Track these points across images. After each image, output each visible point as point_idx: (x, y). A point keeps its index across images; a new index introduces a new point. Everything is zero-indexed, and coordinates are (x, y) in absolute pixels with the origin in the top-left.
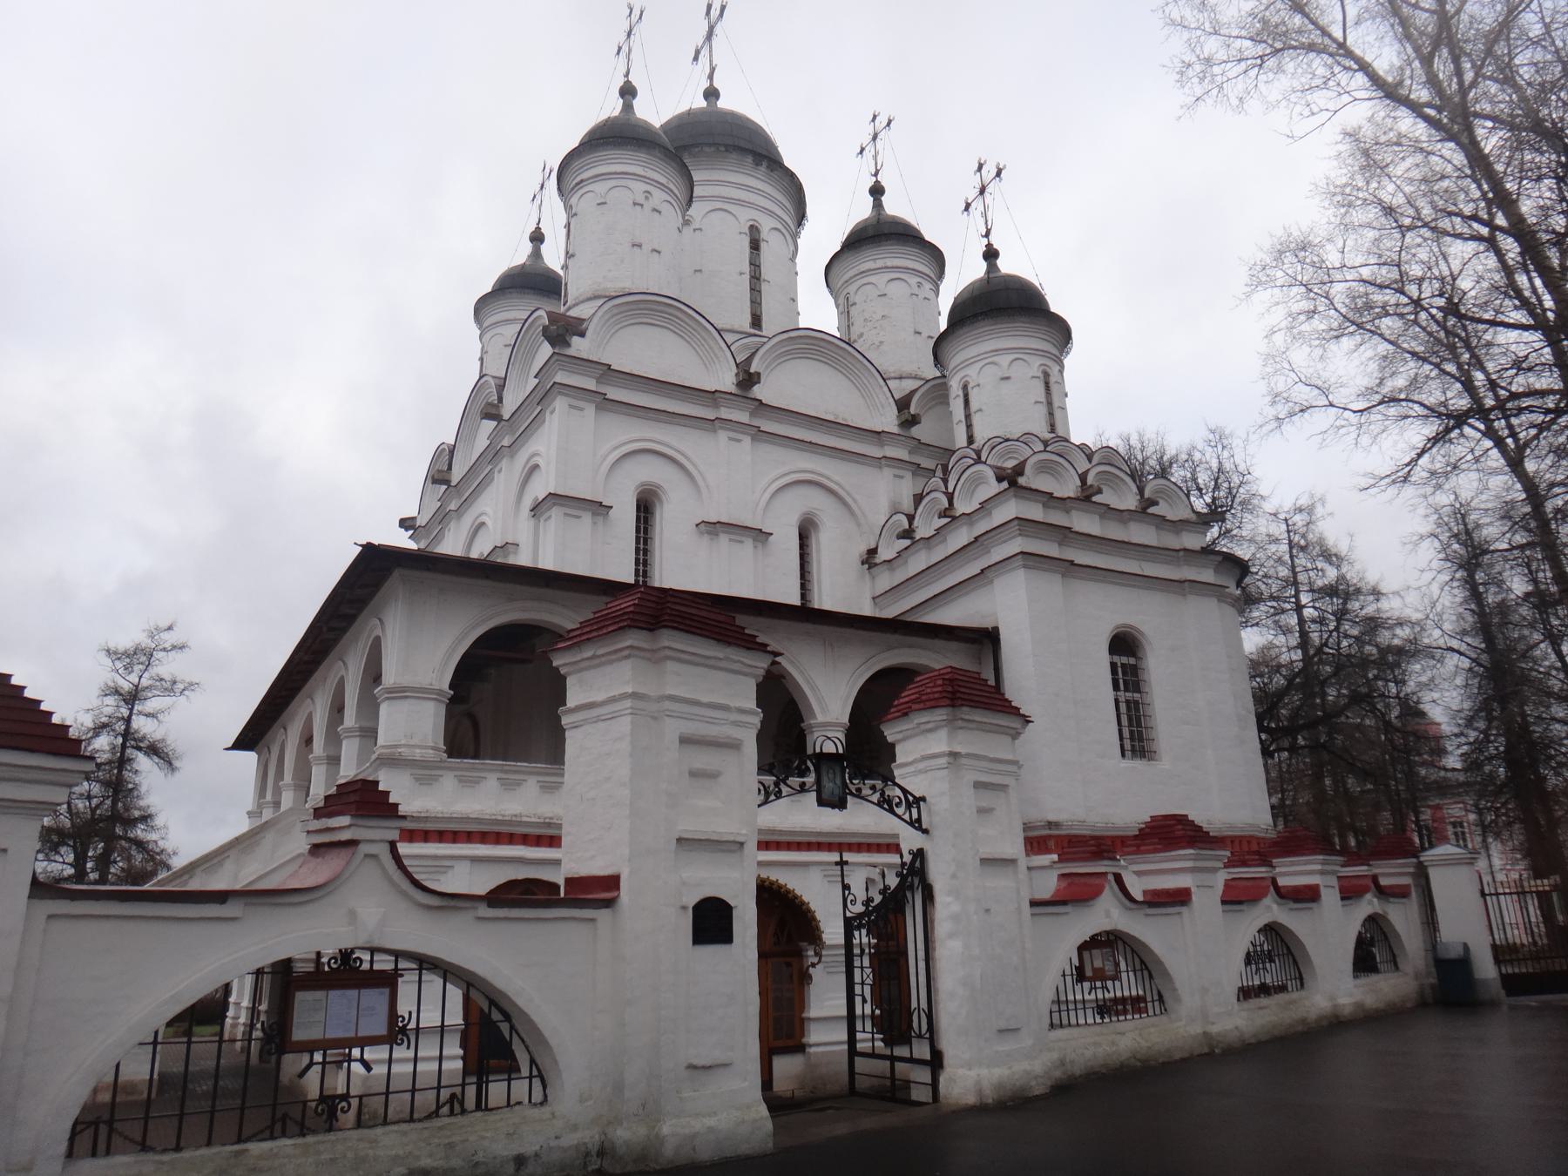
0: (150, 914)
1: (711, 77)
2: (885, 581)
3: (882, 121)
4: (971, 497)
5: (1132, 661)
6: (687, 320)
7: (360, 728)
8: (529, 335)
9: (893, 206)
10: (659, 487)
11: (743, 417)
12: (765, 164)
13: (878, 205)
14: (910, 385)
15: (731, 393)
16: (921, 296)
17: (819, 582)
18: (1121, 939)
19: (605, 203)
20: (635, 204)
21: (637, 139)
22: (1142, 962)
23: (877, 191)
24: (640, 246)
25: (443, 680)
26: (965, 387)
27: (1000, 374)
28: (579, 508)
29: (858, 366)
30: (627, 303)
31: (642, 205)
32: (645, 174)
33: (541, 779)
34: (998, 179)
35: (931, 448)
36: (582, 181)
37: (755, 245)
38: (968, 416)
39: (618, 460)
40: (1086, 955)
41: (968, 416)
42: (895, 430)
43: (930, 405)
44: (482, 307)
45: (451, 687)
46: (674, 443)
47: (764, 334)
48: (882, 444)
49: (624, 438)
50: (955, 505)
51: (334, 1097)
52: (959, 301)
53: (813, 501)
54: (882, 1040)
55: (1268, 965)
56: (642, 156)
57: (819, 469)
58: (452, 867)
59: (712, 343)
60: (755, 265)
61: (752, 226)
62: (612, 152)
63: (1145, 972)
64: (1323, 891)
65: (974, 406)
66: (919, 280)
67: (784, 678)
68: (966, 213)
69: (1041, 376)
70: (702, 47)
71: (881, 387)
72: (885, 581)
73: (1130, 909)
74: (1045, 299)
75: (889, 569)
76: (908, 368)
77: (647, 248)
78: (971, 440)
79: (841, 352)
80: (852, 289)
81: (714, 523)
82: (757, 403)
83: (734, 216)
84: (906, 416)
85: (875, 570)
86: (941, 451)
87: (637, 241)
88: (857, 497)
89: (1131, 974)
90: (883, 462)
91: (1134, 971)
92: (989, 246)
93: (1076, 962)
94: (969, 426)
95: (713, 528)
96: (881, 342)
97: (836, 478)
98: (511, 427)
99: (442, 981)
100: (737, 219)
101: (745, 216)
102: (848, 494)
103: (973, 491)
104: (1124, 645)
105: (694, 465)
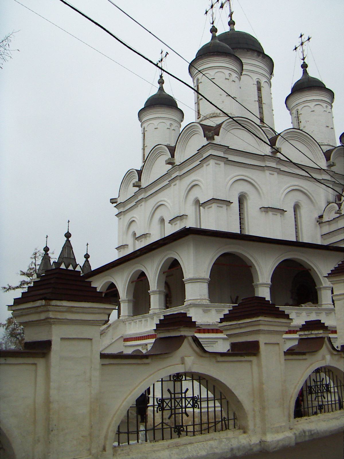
0: (230, 360)
1: (231, 16)
7: (159, 291)
8: (187, 132)
9: (312, 73)
10: (246, 194)
11: (274, 165)
13: (305, 72)
14: (329, 148)
15: (269, 156)
17: (301, 229)
21: (226, 53)
23: (304, 66)
25: (206, 275)
29: (311, 142)
33: (216, 309)
37: (259, 89)
39: (287, 193)
42: (325, 168)
43: (337, 156)
44: (141, 113)
45: (271, 282)
46: (251, 176)
48: (264, 161)
49: (233, 175)
51: (179, 426)
55: (313, 384)
56: (227, 59)
57: (301, 185)
58: (217, 342)
60: (260, 97)
62: (216, 58)
64: (262, 347)
67: (310, 270)
70: (225, 3)
72: (326, 229)
75: (328, 224)
79: (305, 137)
80: (299, 108)
81: (267, 208)
84: (329, 164)
85: (322, 225)
88: (313, 195)
90: (266, 168)
91: (337, 387)
95: (266, 209)
97: (306, 188)
98: (179, 168)
101: (255, 77)
102: (310, 194)
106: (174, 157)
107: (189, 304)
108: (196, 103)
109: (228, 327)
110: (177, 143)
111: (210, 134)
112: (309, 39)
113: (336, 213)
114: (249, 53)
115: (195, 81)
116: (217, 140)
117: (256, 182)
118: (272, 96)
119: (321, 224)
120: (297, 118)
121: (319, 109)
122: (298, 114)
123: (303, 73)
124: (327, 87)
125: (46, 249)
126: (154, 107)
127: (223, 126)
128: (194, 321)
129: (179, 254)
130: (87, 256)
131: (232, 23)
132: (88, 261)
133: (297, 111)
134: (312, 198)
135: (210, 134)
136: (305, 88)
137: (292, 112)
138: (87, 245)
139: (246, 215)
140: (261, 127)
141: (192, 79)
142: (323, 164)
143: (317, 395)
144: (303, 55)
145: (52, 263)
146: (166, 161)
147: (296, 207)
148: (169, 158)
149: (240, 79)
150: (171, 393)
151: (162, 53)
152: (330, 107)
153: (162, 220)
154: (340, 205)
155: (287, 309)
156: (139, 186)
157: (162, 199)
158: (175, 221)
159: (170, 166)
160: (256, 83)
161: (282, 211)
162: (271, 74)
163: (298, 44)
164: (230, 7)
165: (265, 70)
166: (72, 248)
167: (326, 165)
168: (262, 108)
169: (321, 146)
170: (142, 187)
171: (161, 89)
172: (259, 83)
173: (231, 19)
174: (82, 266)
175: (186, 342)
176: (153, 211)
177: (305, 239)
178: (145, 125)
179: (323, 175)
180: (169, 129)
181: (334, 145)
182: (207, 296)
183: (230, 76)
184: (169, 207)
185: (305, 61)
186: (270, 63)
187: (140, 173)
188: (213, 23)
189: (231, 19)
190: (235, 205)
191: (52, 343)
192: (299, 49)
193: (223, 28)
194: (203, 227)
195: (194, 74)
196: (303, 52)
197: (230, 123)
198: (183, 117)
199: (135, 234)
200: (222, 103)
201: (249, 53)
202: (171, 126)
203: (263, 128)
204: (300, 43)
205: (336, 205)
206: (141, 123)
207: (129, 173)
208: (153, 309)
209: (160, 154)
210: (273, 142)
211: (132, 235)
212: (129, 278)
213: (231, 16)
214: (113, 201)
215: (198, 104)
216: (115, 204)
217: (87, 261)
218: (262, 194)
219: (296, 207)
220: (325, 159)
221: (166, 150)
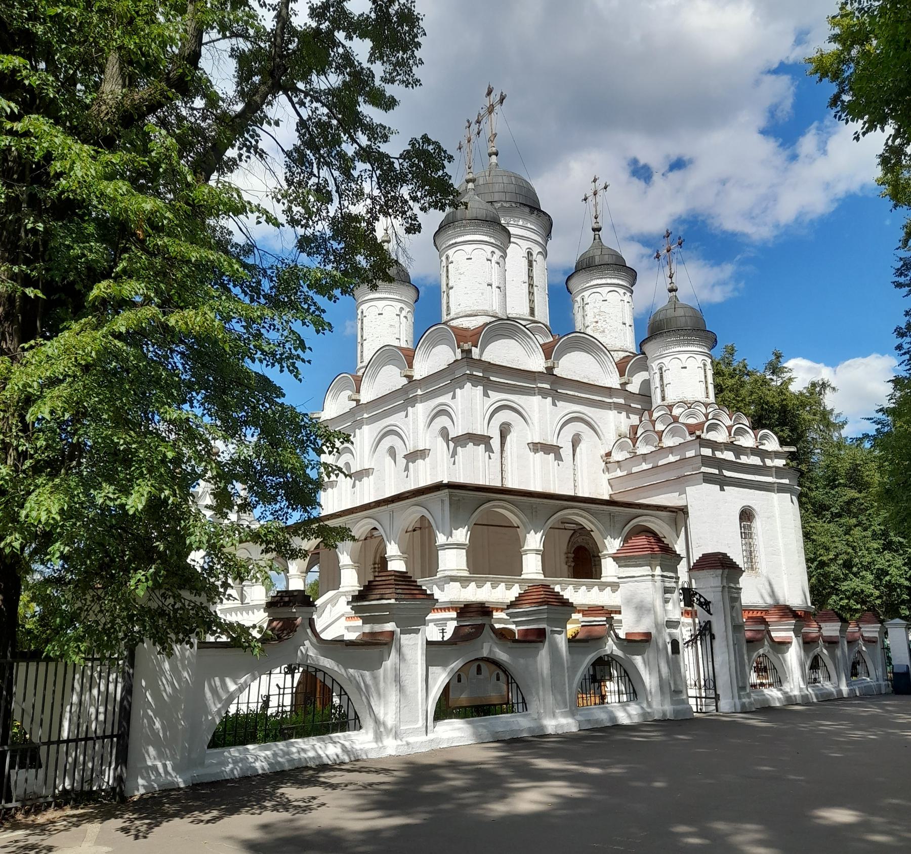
3: (600, 184)
12: (535, 212)
13: (597, 239)
14: (622, 355)
22: (625, 672)
36: (456, 243)
40: (597, 668)
41: (662, 385)
46: (516, 401)
47: (536, 319)
48: (611, 397)
53: (579, 427)
54: (293, 753)
57: (585, 412)
63: (627, 678)
69: (702, 366)
76: (618, 345)
78: (663, 399)
80: (586, 294)
88: (599, 424)
93: (591, 673)
94: (663, 391)
104: (746, 515)
107: (444, 575)
109: (718, 660)
143: (281, 700)
144: (596, 211)
150: (279, 688)
160: (526, 255)
163: (590, 194)
169: (612, 353)
172: (530, 254)
182: (464, 566)
190: (495, 443)
196: (596, 205)
205: (629, 441)
218: (529, 421)
220: (618, 374)
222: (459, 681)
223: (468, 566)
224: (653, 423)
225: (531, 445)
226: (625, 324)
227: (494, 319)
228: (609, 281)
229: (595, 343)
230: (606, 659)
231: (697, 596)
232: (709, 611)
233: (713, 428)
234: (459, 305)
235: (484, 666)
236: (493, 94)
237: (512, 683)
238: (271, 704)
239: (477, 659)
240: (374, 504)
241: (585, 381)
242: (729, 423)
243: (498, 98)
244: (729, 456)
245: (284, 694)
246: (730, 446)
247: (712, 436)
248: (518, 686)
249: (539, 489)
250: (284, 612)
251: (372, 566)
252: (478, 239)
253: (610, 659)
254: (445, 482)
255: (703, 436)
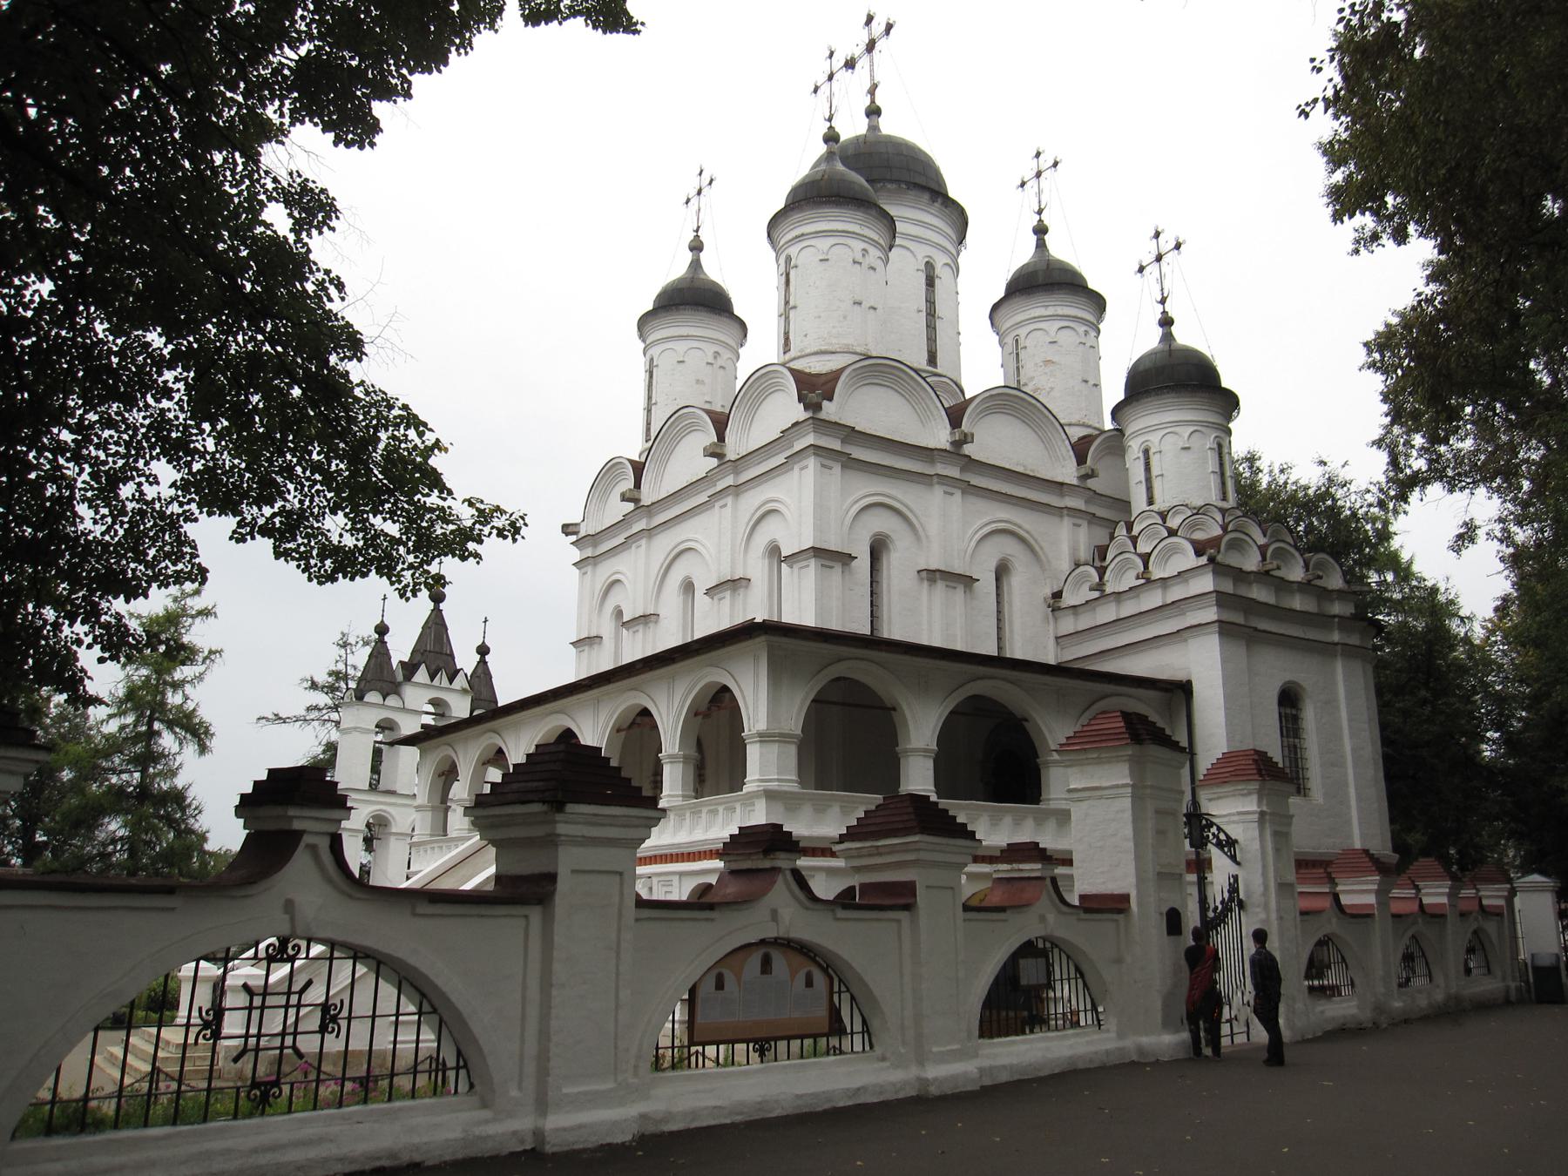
1: (872, 91)
2: (1068, 625)
4: (1166, 562)
5: (1294, 712)
6: (908, 381)
9: (1058, 249)
10: (887, 536)
11: (954, 472)
13: (1041, 245)
14: (1083, 432)
16: (1088, 345)
18: (1057, 946)
19: (827, 260)
20: (855, 262)
24: (860, 304)
26: (1146, 452)
27: (1181, 444)
28: (831, 560)
30: (862, 367)
31: (860, 263)
32: (862, 233)
34: (1176, 251)
35: (1103, 498)
36: (803, 235)
37: (930, 282)
38: (1149, 480)
41: (1149, 480)
42: (1075, 482)
44: (645, 322)
46: (900, 496)
47: (939, 370)
48: (932, 462)
50: (1150, 568)
52: (1141, 368)
53: (1009, 547)
56: (860, 215)
57: (1019, 521)
59: (929, 402)
60: (931, 303)
61: (927, 263)
63: (1080, 981)
65: (1155, 471)
66: (1085, 328)
68: (1139, 275)
71: (1063, 441)
72: (1068, 625)
73: (807, 909)
74: (1216, 370)
77: (866, 305)
78: (1151, 502)
80: (1023, 332)
82: (966, 459)
83: (911, 252)
84: (1083, 471)
86: (1111, 500)
87: (858, 299)
88: (1043, 544)
89: (1066, 982)
92: (1164, 312)
94: (1150, 489)
95: (932, 576)
96: (1052, 389)
97: (1027, 526)
99: (396, 992)
100: (915, 256)
101: (923, 252)
103: (1168, 559)
105: (915, 516)
106: (724, 441)
108: (780, 316)
110: (734, 409)
111: (813, 397)
112: (1055, 164)
113: (1091, 589)
114: (912, 194)
115: (782, 261)
116: (830, 410)
117: (911, 511)
118: (961, 338)
119: (1056, 613)
120: (1014, 355)
121: (1067, 338)
122: (1017, 346)
123: (1037, 247)
124: (1090, 286)
125: (382, 630)
126: (677, 310)
127: (843, 378)
128: (626, 776)
129: (735, 675)
130: (483, 650)
131: (873, 112)
132: (486, 663)
133: (1017, 340)
134: (1037, 548)
135: (813, 397)
136: (1039, 286)
137: (1005, 341)
138: (485, 622)
139: (885, 586)
140: (924, 375)
141: (774, 254)
142: (1067, 471)
145: (395, 663)
146: (704, 449)
147: (1002, 572)
148: (714, 443)
149: (886, 261)
151: (700, 174)
152: (1093, 334)
153: (688, 587)
154: (1102, 571)
155: (962, 810)
156: (636, 501)
157: (691, 536)
158: (721, 592)
159: (714, 462)
160: (923, 267)
161: (968, 581)
162: (961, 243)
164: (872, 70)
165: (947, 236)
166: (447, 629)
167: (1076, 474)
168: (935, 328)
169: (1066, 428)
170: (642, 504)
171: (696, 265)
172: (929, 266)
173: (873, 101)
174: (469, 675)
175: (780, 879)
176: (667, 562)
177: (1018, 651)
178: (654, 351)
179: (1067, 498)
180: (712, 364)
181: (1097, 425)
183: (863, 255)
184: (707, 557)
185: (1043, 216)
186: (958, 219)
187: (638, 468)
188: (830, 120)
189: (873, 101)
190: (863, 563)
191: (559, 877)
192: (1032, 186)
193: (852, 127)
194: (787, 618)
195: (781, 244)
196: (1039, 193)
197: (859, 372)
198: (746, 336)
199: (619, 613)
200: (841, 319)
201: (910, 192)
202: (715, 358)
203: (929, 380)
204: (1034, 173)
206: (643, 345)
207: (610, 470)
208: (669, 796)
209: (692, 428)
210: (955, 416)
211: (612, 614)
212: (613, 721)
213: (872, 91)
214: (567, 529)
215: (787, 319)
216: (574, 538)
217: (483, 663)
219: (1002, 572)
220: (1074, 460)
221: (706, 423)
222: (720, 985)
223: (936, 786)
224: (1134, 540)
225: (924, 574)
226: (1086, 381)
227: (858, 358)
228: (1061, 311)
229: (1035, 407)
230: (1041, 945)
231: (1214, 830)
232: (1233, 858)
233: (1235, 545)
234: (806, 336)
235: (779, 961)
236: (874, 23)
237: (840, 992)
238: (227, 1030)
239: (763, 942)
240: (640, 665)
241: (1020, 469)
242: (1261, 541)
243: (883, 27)
244: (1259, 593)
245: (263, 1008)
246: (1264, 576)
247: (1234, 560)
248: (853, 998)
249: (937, 642)
250: (273, 817)
251: (652, 778)
252: (840, 229)
253: (1048, 945)
254: (759, 620)
255: (1219, 558)
